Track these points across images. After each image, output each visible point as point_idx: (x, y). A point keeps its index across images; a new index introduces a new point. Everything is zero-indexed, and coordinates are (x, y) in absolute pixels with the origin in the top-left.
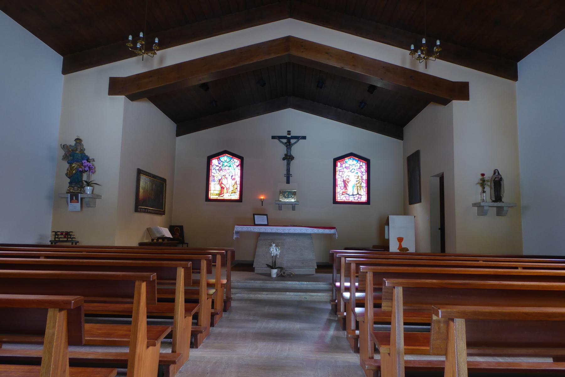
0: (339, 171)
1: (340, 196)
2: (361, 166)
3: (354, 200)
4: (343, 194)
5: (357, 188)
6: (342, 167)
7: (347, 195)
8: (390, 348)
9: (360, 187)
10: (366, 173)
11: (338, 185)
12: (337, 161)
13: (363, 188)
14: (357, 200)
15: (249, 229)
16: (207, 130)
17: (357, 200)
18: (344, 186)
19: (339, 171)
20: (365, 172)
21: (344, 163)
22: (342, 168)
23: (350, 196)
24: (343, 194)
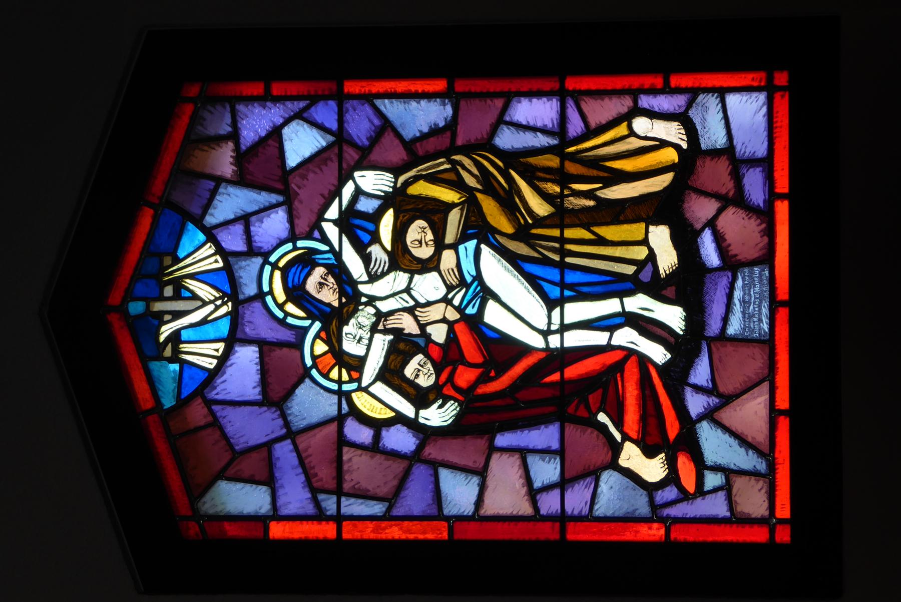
0: (329, 504)
1: (712, 480)
2: (241, 158)
3: (767, 258)
4: (673, 429)
5: (586, 219)
6: (268, 445)
7: (701, 373)
8: (639, 455)
9: (564, 178)
10: (352, 87)
11: (550, 503)
12: (193, 530)
13: (575, 126)
14: (766, 215)
15: (287, 529)
16: (388, 276)
17: (766, 215)
18: (563, 418)
19: (329, 504)
20: (341, 98)
21: (215, 423)
22: (284, 452)
23: (713, 327)
24: (673, 429)
